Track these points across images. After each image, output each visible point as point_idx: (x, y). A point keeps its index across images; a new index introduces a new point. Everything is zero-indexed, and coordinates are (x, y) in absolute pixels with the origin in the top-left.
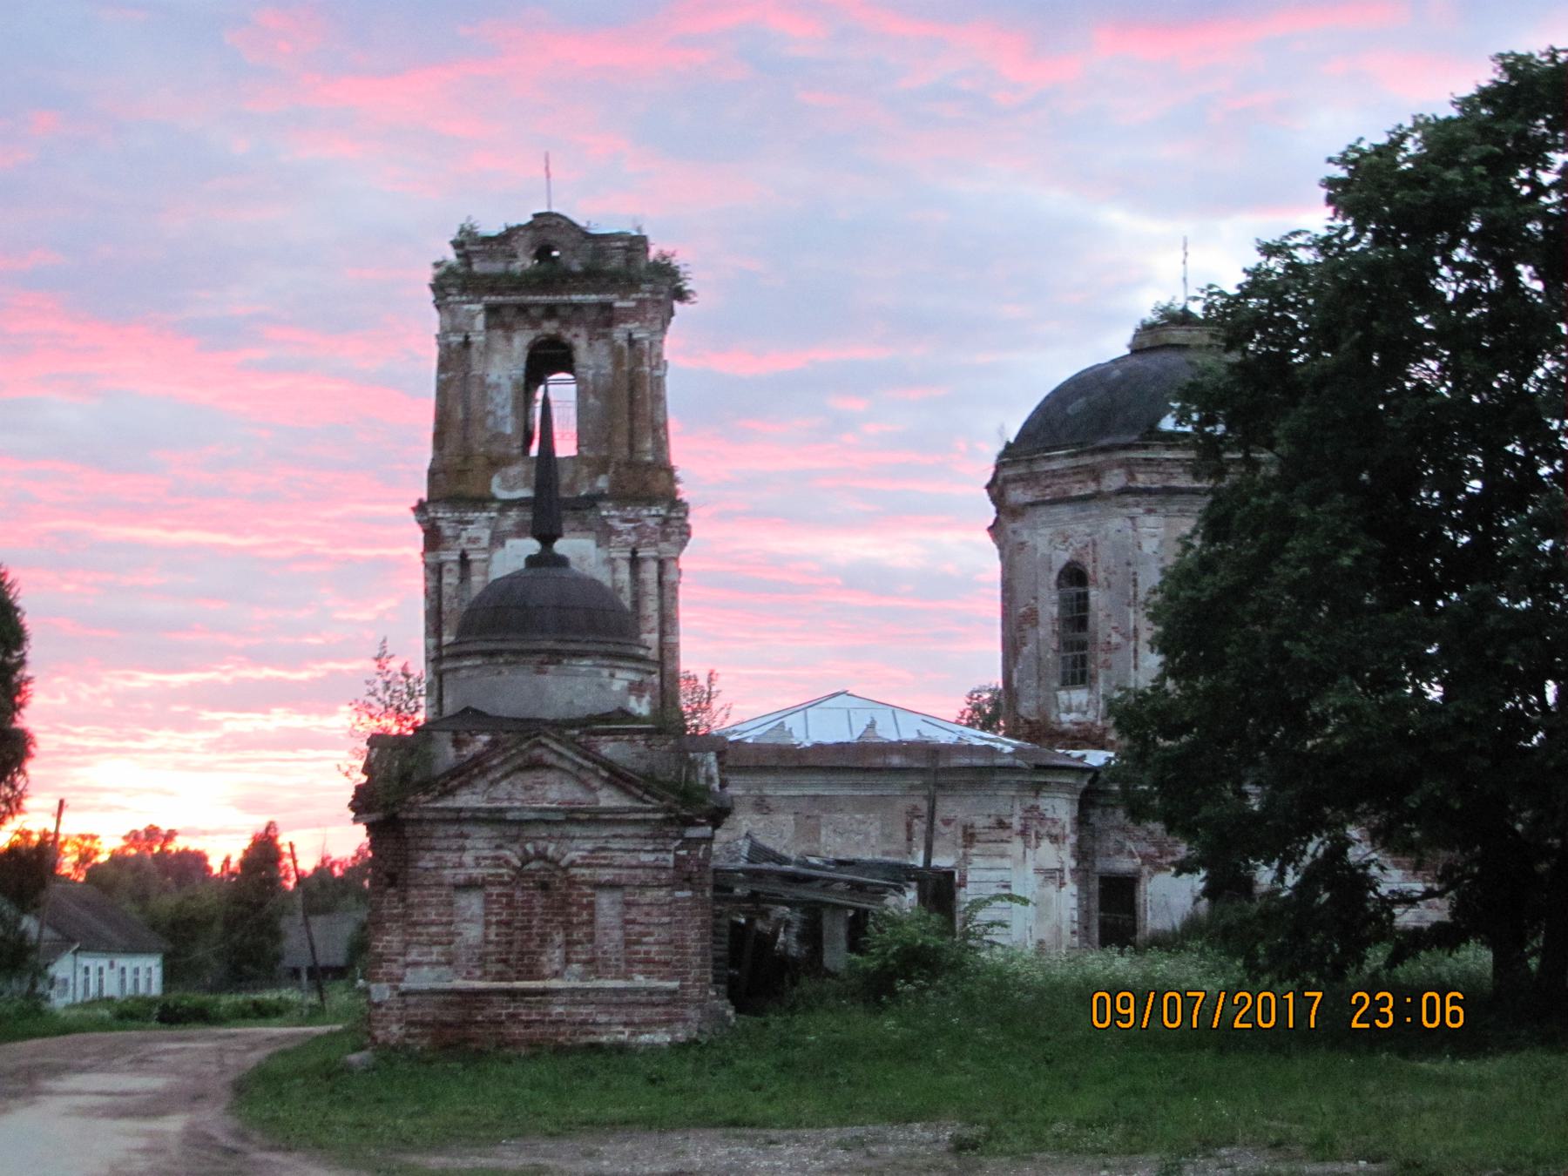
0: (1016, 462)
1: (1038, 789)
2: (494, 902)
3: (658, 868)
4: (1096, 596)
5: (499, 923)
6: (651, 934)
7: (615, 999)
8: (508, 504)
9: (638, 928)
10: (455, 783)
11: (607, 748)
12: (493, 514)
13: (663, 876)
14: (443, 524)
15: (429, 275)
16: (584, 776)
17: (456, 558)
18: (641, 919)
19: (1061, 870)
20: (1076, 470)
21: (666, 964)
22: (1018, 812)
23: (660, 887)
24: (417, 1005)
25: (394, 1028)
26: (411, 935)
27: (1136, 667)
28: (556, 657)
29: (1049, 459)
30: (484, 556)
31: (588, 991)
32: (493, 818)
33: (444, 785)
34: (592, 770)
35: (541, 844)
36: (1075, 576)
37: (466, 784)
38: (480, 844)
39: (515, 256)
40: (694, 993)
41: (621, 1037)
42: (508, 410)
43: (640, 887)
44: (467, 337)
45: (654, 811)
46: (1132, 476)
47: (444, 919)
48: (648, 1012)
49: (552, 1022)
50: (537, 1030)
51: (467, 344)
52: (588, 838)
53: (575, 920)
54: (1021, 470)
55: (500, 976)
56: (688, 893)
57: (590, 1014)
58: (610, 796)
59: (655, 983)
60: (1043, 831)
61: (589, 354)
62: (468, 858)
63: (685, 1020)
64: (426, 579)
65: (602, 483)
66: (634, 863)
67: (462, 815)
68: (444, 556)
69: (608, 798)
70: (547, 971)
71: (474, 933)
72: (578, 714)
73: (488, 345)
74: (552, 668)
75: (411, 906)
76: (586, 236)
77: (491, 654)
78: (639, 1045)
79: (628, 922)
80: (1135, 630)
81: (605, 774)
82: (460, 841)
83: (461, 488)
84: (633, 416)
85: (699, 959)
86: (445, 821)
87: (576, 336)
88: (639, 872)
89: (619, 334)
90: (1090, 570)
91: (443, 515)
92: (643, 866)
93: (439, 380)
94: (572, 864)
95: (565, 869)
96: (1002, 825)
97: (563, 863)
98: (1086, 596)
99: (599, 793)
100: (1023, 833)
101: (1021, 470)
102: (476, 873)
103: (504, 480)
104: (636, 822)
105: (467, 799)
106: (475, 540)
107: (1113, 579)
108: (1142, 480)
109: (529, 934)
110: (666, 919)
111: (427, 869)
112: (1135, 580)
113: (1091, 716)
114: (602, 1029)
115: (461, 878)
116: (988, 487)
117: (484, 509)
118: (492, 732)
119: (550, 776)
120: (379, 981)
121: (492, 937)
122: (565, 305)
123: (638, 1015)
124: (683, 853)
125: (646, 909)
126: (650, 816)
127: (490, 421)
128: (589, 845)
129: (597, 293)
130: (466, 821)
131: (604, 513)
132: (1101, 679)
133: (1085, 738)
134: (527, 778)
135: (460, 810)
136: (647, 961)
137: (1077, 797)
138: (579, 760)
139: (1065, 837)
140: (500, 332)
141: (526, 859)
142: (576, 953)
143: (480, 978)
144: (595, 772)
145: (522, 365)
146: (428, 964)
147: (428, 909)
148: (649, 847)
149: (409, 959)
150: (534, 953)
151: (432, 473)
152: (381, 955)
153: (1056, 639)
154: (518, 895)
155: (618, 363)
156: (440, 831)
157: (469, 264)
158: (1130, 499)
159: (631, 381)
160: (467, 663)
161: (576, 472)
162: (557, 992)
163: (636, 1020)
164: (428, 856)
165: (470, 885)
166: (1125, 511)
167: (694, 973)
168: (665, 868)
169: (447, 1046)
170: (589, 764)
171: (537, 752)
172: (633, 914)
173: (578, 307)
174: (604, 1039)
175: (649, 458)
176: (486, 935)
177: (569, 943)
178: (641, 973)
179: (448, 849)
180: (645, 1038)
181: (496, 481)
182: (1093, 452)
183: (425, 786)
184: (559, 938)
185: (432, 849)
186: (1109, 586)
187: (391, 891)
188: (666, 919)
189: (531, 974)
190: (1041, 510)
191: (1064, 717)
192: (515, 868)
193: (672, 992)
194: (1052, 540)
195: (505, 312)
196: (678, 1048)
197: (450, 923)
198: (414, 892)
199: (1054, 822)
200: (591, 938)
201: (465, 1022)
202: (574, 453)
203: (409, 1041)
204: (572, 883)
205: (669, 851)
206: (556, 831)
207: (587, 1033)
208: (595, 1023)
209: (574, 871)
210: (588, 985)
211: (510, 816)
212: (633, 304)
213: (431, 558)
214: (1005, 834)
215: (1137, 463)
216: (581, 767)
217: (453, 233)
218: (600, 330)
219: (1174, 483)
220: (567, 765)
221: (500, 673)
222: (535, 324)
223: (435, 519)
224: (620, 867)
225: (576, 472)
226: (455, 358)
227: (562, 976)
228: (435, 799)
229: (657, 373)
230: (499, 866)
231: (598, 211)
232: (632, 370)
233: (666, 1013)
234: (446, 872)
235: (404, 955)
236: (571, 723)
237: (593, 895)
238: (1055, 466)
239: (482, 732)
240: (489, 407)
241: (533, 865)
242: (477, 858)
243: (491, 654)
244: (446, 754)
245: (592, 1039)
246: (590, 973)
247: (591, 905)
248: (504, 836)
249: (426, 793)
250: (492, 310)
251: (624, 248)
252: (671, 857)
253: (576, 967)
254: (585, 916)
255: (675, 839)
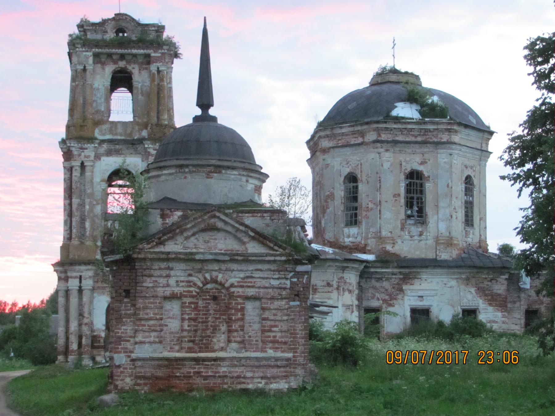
0: (325, 129)
1: (344, 269)
2: (187, 307)
3: (281, 288)
4: (362, 187)
5: (190, 319)
6: (276, 326)
7: (256, 363)
8: (103, 141)
9: (269, 323)
10: (165, 237)
11: (249, 220)
12: (96, 145)
13: (284, 293)
14: (73, 149)
15: (67, 39)
16: (239, 235)
17: (79, 164)
18: (272, 317)
19: (352, 305)
20: (353, 133)
21: (285, 343)
22: (336, 279)
23: (282, 299)
24: (142, 367)
25: (128, 380)
26: (138, 326)
27: (380, 218)
28: (218, 169)
29: (341, 128)
30: (92, 164)
31: (240, 359)
32: (188, 258)
33: (160, 238)
34: (245, 232)
35: (214, 274)
36: (352, 179)
37: (171, 238)
38: (179, 273)
39: (107, 32)
40: (301, 360)
41: (260, 385)
42: (103, 100)
43: (271, 299)
44: (85, 67)
45: (281, 255)
46: (379, 135)
47: (158, 317)
48: (275, 371)
49: (220, 377)
50: (211, 382)
51: (85, 70)
52: (241, 271)
53: (233, 318)
54: (328, 132)
55: (190, 350)
56: (298, 303)
57: (243, 372)
58: (254, 247)
59: (279, 354)
60: (346, 288)
61: (140, 78)
62: (172, 281)
63: (296, 376)
64: (65, 174)
65: (145, 133)
66: (267, 285)
67: (170, 256)
68: (74, 163)
69: (254, 248)
70: (216, 347)
71: (174, 325)
72: (230, 202)
73: (94, 70)
74: (215, 175)
75: (139, 309)
76: (138, 24)
77: (181, 166)
78: (270, 390)
79: (264, 319)
80: (380, 201)
81: (252, 234)
82: (168, 272)
83: (82, 133)
84: (159, 103)
85: (303, 341)
86: (160, 260)
87: (133, 68)
88: (270, 290)
89: (153, 68)
90: (359, 176)
91: (74, 145)
92: (273, 287)
93: (71, 86)
94: (232, 285)
95: (228, 289)
96: (329, 285)
97: (227, 285)
98: (357, 187)
99: (247, 245)
100: (338, 289)
101: (328, 132)
102: (177, 290)
103: (101, 131)
104: (269, 262)
105: (171, 247)
106: (88, 157)
107: (370, 180)
108: (384, 137)
109: (207, 326)
110: (285, 318)
111: (148, 287)
112: (380, 180)
113: (359, 239)
114: (249, 381)
115: (168, 293)
116: (308, 142)
117: (93, 143)
118: (183, 210)
119: (220, 235)
120: (120, 352)
121: (186, 327)
122: (129, 54)
123: (270, 372)
124: (295, 280)
125: (274, 311)
126: (278, 258)
127: (94, 105)
128: (242, 275)
129: (144, 49)
130: (173, 259)
131: (146, 146)
132: (364, 223)
133: (356, 249)
134: (206, 236)
135: (169, 253)
136: (274, 342)
137: (359, 273)
138: (237, 225)
139: (354, 291)
140: (99, 65)
141: (205, 283)
142: (234, 337)
143: (178, 351)
144: (246, 233)
145: (110, 80)
146: (149, 342)
147: (148, 311)
148: (276, 276)
149: (137, 340)
150: (209, 336)
151: (68, 127)
152: (120, 337)
153: (343, 206)
154: (201, 303)
155: (153, 80)
156: (156, 265)
157: (86, 35)
158: (379, 145)
159: (158, 89)
160: (165, 172)
161: (133, 128)
162: (223, 359)
163: (269, 375)
164: (148, 280)
165: (173, 297)
166: (376, 150)
167: (301, 348)
168: (285, 289)
169: (160, 390)
170: (241, 228)
171: (213, 220)
172: (267, 314)
173: (135, 56)
174: (250, 386)
175: (166, 123)
176: (182, 326)
177: (230, 331)
178: (270, 348)
179: (161, 276)
180: (274, 386)
181: (97, 131)
182: (362, 125)
183: (148, 239)
184: (224, 328)
185: (150, 276)
186: (368, 183)
187: (126, 300)
188: (285, 318)
189: (207, 348)
190: (337, 150)
191: (347, 240)
192: (199, 287)
193: (288, 360)
194: (340, 163)
195: (102, 56)
196: (291, 390)
197: (161, 319)
198: (141, 301)
199: (350, 284)
200: (242, 328)
201: (169, 376)
202: (132, 120)
203: (137, 388)
204: (231, 296)
205: (287, 279)
206: (223, 266)
207: (241, 383)
208: (245, 377)
209: (232, 290)
210: (241, 355)
211: (198, 257)
212: (160, 55)
213: (68, 164)
214: (330, 289)
215: (382, 129)
216: (238, 230)
217: (78, 21)
218: (144, 66)
219: (397, 138)
220: (229, 229)
221: (185, 178)
222: (115, 62)
223: (69, 147)
224: (259, 288)
225: (133, 128)
226: (79, 77)
227: (224, 349)
228: (152, 247)
229: (169, 86)
230: (191, 286)
231: (145, 15)
232: (159, 84)
233: (286, 372)
234: (159, 289)
235: (134, 337)
236: (229, 207)
237: (244, 303)
238: (343, 131)
239: (178, 210)
240: (94, 98)
241: (209, 286)
242: (177, 282)
243: (181, 166)
244: (156, 222)
245: (243, 386)
246: (241, 348)
247: (243, 309)
248: (193, 269)
249: (147, 244)
250: (96, 56)
251: (156, 30)
252: (288, 282)
253: (234, 345)
254: (239, 315)
255: (291, 272)
